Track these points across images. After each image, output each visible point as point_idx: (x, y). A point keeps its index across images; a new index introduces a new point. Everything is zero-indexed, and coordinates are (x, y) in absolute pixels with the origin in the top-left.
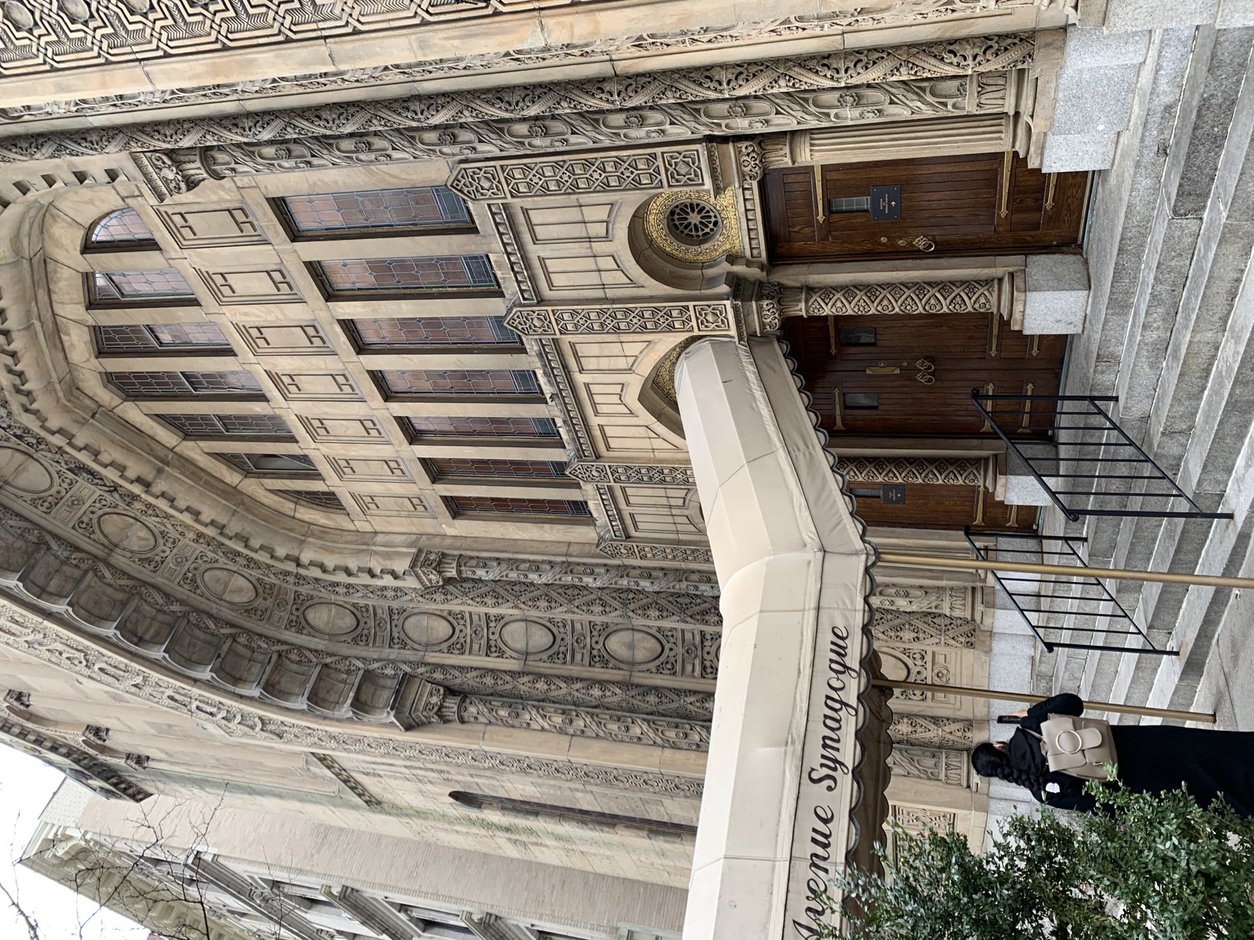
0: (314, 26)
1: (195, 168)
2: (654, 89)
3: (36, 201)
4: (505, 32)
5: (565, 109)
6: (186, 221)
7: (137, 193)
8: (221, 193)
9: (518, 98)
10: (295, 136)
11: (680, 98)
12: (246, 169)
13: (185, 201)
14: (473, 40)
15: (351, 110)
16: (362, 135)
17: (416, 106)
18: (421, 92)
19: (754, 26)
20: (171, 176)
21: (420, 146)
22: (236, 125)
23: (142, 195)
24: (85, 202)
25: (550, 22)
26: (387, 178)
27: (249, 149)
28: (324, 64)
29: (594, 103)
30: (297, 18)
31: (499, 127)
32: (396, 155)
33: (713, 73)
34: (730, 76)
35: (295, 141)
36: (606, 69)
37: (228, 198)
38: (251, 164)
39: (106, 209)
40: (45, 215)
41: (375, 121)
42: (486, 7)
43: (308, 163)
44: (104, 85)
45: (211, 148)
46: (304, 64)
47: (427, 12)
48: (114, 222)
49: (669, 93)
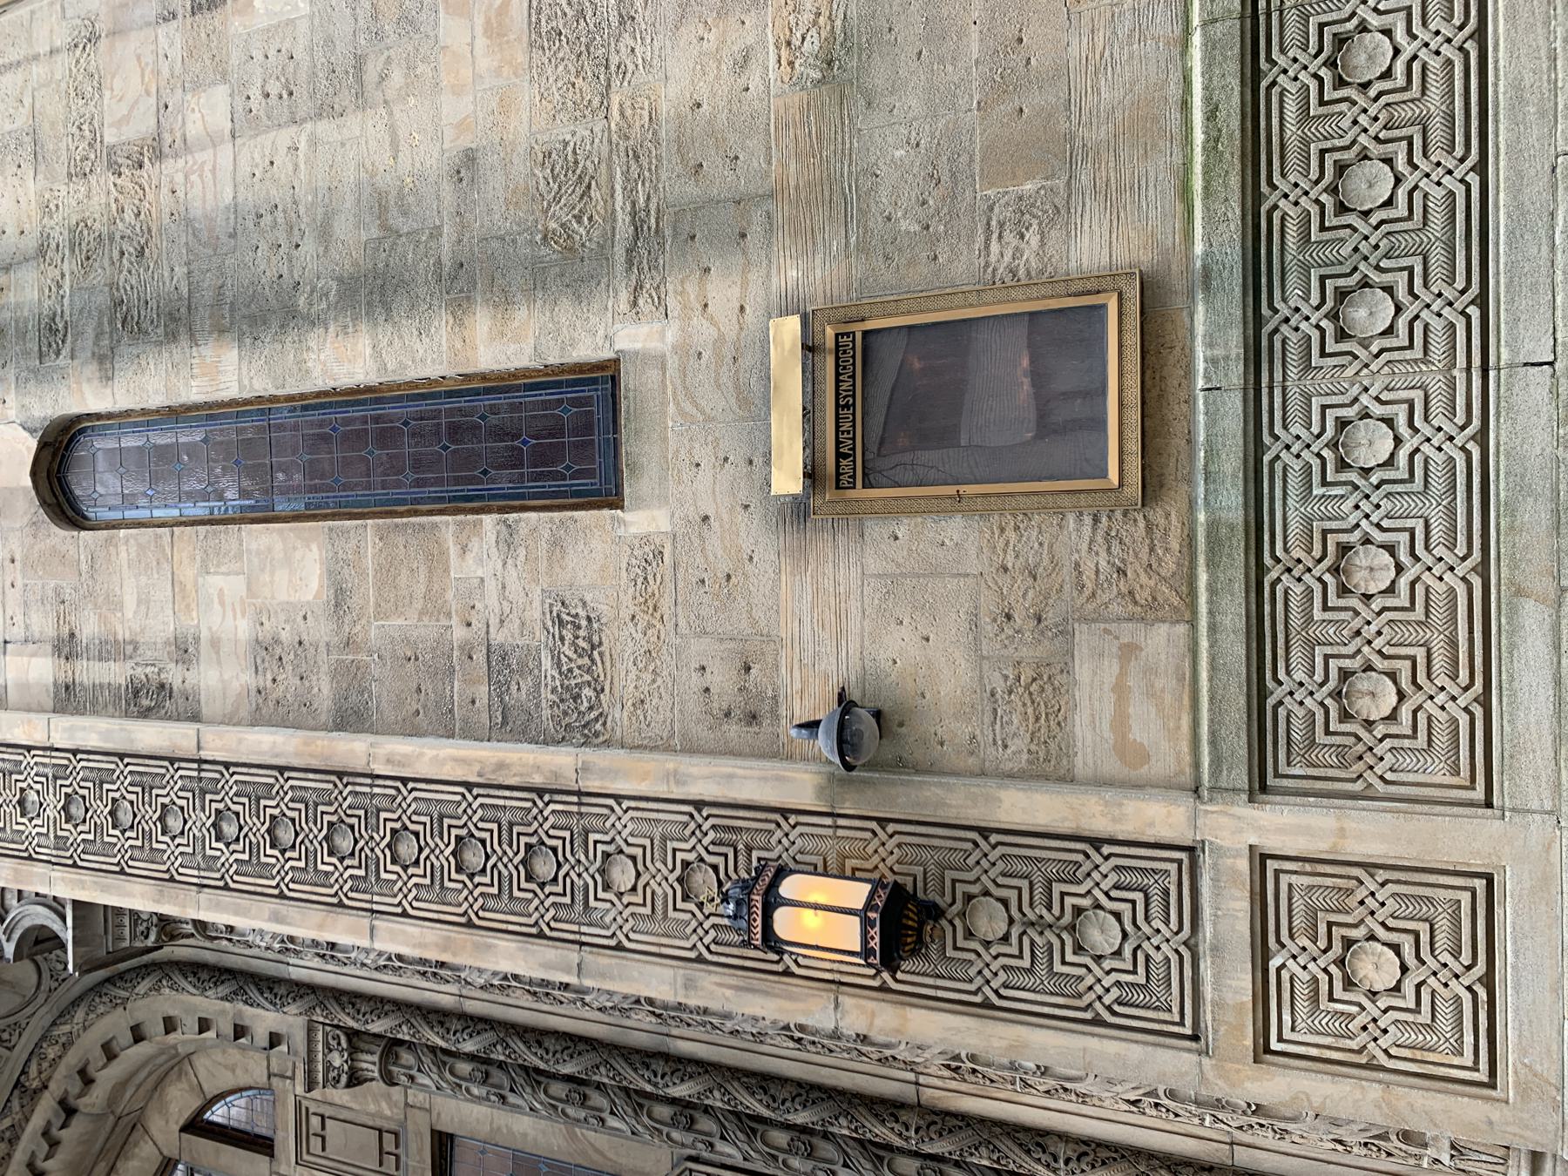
0: (575, 928)
1: (369, 1063)
2: (965, 1138)
3: (175, 1047)
4: (790, 997)
5: (842, 1129)
6: (323, 1128)
7: (289, 1074)
8: (384, 1105)
9: (787, 1095)
10: (502, 1058)
11: (998, 1162)
12: (427, 1081)
13: (337, 1101)
14: (750, 996)
15: (581, 1047)
16: (582, 1082)
17: (659, 1066)
18: (672, 1051)
19: (1108, 1086)
20: (337, 1063)
21: (645, 1119)
22: (442, 1024)
23: (293, 1078)
24: (226, 1067)
25: (847, 1001)
26: (591, 1152)
27: (442, 1057)
28: (569, 972)
29: (883, 1132)
30: (562, 914)
31: (752, 1125)
32: (612, 1122)
33: (1048, 1141)
34: (1070, 1153)
35: (501, 1065)
36: (909, 1093)
37: (388, 1113)
38: (435, 1077)
39: (242, 1082)
40: (177, 1064)
41: (602, 1069)
42: (777, 962)
43: (503, 1098)
44: (277, 918)
45: (401, 1042)
46: (547, 966)
47: (708, 948)
48: (242, 1102)
49: (983, 1151)
